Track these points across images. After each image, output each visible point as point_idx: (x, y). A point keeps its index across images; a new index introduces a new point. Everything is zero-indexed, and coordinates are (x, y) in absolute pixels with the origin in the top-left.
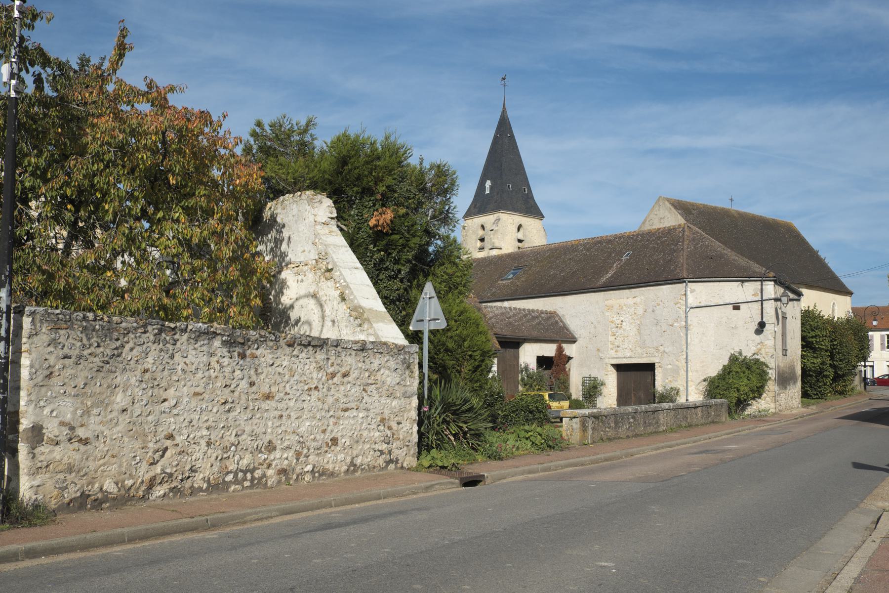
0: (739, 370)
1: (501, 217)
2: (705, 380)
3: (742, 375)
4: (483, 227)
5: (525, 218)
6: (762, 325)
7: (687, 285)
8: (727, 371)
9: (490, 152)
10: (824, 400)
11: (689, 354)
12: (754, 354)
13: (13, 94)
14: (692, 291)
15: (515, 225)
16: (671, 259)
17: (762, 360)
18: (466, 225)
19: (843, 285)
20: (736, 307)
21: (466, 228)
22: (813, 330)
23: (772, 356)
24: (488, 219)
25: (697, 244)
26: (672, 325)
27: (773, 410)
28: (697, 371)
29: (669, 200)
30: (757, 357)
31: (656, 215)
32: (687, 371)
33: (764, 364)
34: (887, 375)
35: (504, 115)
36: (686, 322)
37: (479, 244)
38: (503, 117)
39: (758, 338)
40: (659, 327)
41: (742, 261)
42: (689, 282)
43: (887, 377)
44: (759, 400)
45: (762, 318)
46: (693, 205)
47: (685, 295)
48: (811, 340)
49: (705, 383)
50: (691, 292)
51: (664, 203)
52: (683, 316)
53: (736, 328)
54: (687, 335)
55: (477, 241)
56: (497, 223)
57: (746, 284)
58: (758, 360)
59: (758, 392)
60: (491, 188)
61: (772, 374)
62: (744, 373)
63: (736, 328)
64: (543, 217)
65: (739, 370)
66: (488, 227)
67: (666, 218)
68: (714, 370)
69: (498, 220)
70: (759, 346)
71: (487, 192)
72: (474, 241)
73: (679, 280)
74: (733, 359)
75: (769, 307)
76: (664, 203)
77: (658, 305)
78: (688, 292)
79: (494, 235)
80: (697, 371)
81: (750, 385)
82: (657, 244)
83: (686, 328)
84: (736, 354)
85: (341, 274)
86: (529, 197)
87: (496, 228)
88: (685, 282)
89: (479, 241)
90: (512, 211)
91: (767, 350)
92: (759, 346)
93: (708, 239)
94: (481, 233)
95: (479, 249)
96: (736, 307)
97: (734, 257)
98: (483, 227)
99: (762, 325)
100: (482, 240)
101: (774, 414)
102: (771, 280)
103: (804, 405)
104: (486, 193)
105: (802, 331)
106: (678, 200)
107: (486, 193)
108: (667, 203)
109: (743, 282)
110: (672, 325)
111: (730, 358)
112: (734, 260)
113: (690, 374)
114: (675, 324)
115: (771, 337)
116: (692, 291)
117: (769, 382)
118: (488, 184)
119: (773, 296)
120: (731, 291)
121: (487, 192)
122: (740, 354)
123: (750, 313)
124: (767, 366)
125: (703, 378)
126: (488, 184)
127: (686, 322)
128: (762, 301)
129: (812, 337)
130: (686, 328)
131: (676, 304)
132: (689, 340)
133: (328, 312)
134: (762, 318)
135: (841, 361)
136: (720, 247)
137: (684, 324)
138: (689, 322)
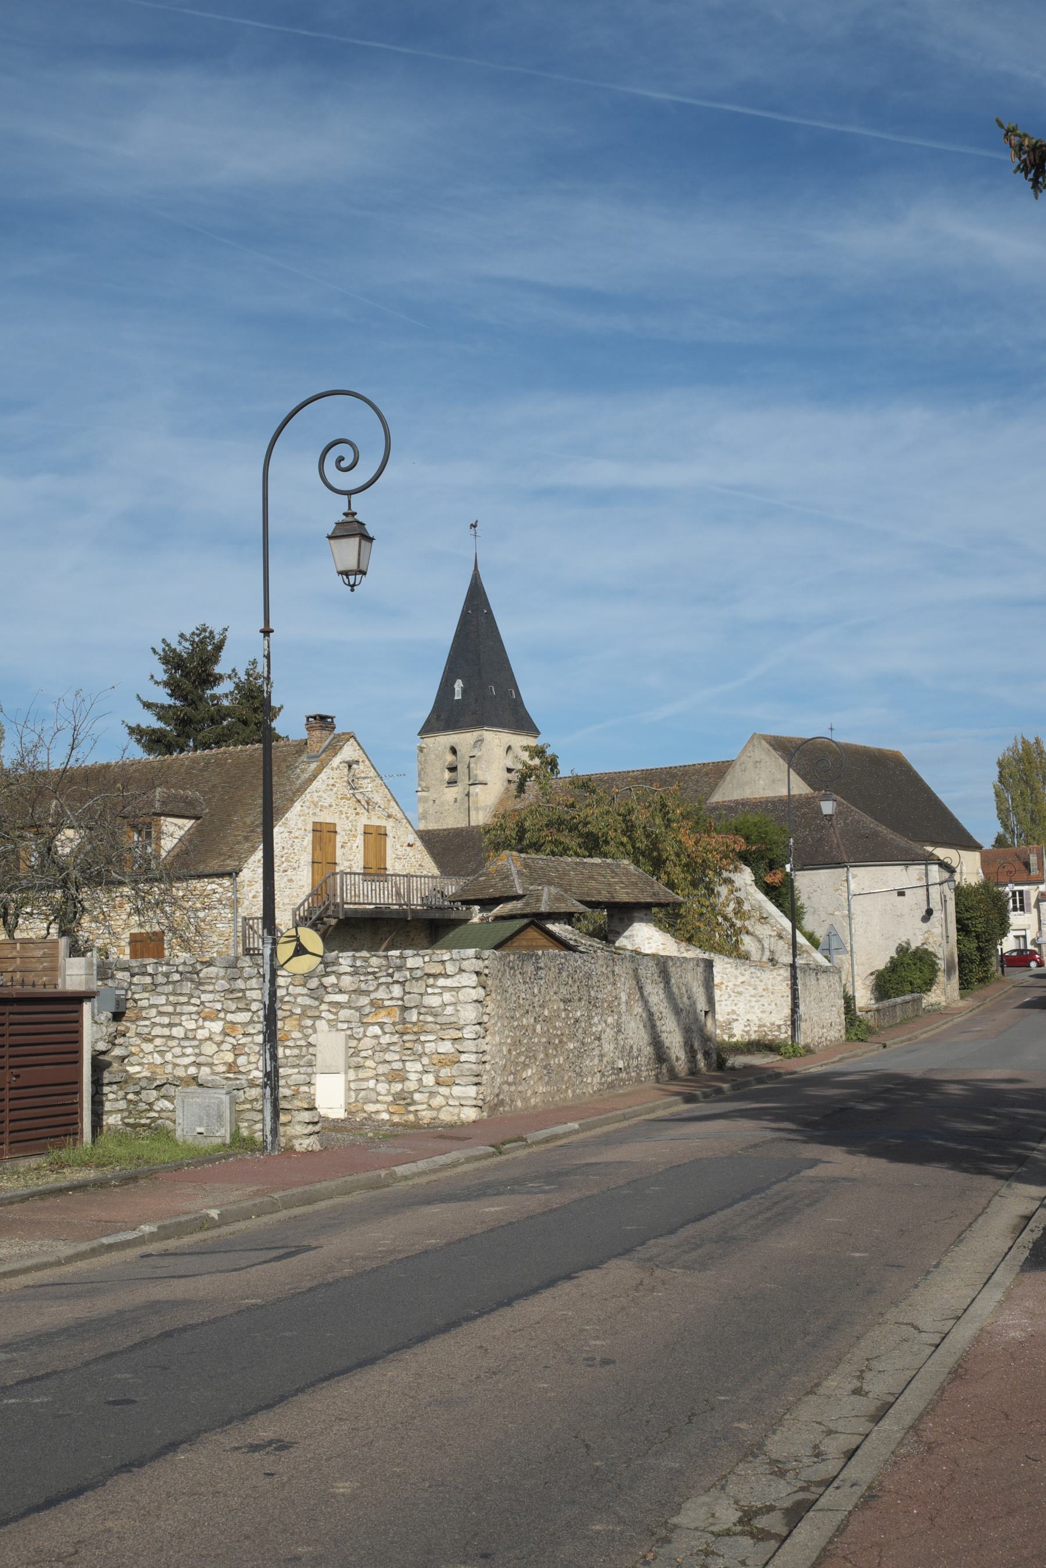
0: (910, 962)
1: (484, 737)
2: (872, 974)
3: (913, 967)
4: (454, 751)
5: (515, 737)
6: (929, 912)
7: (848, 870)
8: (894, 966)
9: (457, 636)
10: (969, 990)
11: (854, 945)
12: (923, 944)
13: (1030, 947)
14: (854, 877)
15: (502, 748)
16: (821, 836)
17: (931, 949)
18: (423, 745)
19: (969, 838)
20: (901, 893)
21: (425, 750)
22: (967, 911)
23: (940, 945)
24: (464, 739)
25: (846, 819)
26: (832, 914)
27: (944, 1004)
28: (863, 964)
29: (765, 738)
30: (925, 947)
31: (750, 757)
32: (852, 965)
33: (932, 953)
34: (1014, 951)
35: (476, 580)
36: (849, 911)
37: (447, 775)
38: (476, 584)
39: (925, 926)
40: (816, 916)
41: (901, 841)
42: (851, 866)
43: (1015, 954)
44: (929, 993)
45: (928, 904)
46: (791, 742)
47: (847, 880)
48: (966, 922)
49: (873, 977)
50: (853, 878)
51: (760, 742)
52: (846, 904)
53: (902, 915)
54: (850, 925)
55: (443, 772)
56: (480, 745)
57: (911, 868)
58: (926, 950)
59: (928, 984)
60: (464, 691)
61: (942, 964)
62: (915, 964)
63: (902, 915)
64: (538, 733)
65: (910, 962)
66: (462, 750)
67: (763, 761)
68: (881, 963)
69: (480, 741)
70: (926, 935)
71: (458, 696)
72: (438, 771)
73: (838, 864)
74: (902, 950)
75: (935, 891)
76: (760, 742)
77: (815, 891)
78: (850, 878)
79: (476, 764)
80: (863, 964)
81: (924, 978)
82: (797, 816)
83: (850, 917)
84: (904, 944)
85: (777, 921)
86: (518, 703)
87: (479, 754)
88: (846, 866)
89: (447, 770)
90: (499, 727)
91: (935, 939)
92: (926, 935)
93: (856, 812)
94: (449, 758)
95: (448, 783)
96: (901, 893)
97: (892, 836)
98: (454, 751)
99: (929, 912)
100: (453, 769)
101: (946, 1007)
102: (935, 864)
103: (962, 997)
104: (456, 698)
105: (957, 912)
106: (774, 737)
107: (456, 698)
108: (764, 743)
109: (907, 865)
110: (832, 914)
111: (897, 949)
112: (891, 839)
113: (856, 967)
114: (836, 913)
115: (938, 925)
116: (854, 877)
117: (939, 973)
118: (459, 685)
119: (938, 881)
120: (896, 875)
121: (458, 696)
122: (908, 943)
123: (915, 900)
124: (936, 956)
125: (870, 972)
126: (459, 685)
127: (849, 911)
128: (928, 885)
129: (968, 919)
130: (850, 917)
131: (836, 891)
132: (853, 930)
133: (766, 946)
134: (928, 904)
135: (987, 941)
136: (872, 822)
137: (847, 912)
138: (852, 910)
